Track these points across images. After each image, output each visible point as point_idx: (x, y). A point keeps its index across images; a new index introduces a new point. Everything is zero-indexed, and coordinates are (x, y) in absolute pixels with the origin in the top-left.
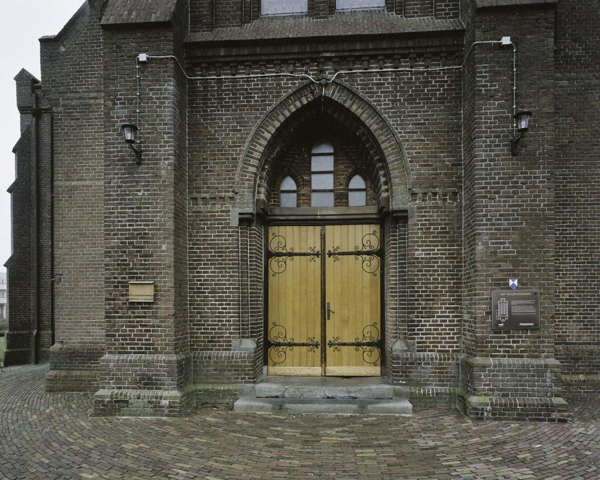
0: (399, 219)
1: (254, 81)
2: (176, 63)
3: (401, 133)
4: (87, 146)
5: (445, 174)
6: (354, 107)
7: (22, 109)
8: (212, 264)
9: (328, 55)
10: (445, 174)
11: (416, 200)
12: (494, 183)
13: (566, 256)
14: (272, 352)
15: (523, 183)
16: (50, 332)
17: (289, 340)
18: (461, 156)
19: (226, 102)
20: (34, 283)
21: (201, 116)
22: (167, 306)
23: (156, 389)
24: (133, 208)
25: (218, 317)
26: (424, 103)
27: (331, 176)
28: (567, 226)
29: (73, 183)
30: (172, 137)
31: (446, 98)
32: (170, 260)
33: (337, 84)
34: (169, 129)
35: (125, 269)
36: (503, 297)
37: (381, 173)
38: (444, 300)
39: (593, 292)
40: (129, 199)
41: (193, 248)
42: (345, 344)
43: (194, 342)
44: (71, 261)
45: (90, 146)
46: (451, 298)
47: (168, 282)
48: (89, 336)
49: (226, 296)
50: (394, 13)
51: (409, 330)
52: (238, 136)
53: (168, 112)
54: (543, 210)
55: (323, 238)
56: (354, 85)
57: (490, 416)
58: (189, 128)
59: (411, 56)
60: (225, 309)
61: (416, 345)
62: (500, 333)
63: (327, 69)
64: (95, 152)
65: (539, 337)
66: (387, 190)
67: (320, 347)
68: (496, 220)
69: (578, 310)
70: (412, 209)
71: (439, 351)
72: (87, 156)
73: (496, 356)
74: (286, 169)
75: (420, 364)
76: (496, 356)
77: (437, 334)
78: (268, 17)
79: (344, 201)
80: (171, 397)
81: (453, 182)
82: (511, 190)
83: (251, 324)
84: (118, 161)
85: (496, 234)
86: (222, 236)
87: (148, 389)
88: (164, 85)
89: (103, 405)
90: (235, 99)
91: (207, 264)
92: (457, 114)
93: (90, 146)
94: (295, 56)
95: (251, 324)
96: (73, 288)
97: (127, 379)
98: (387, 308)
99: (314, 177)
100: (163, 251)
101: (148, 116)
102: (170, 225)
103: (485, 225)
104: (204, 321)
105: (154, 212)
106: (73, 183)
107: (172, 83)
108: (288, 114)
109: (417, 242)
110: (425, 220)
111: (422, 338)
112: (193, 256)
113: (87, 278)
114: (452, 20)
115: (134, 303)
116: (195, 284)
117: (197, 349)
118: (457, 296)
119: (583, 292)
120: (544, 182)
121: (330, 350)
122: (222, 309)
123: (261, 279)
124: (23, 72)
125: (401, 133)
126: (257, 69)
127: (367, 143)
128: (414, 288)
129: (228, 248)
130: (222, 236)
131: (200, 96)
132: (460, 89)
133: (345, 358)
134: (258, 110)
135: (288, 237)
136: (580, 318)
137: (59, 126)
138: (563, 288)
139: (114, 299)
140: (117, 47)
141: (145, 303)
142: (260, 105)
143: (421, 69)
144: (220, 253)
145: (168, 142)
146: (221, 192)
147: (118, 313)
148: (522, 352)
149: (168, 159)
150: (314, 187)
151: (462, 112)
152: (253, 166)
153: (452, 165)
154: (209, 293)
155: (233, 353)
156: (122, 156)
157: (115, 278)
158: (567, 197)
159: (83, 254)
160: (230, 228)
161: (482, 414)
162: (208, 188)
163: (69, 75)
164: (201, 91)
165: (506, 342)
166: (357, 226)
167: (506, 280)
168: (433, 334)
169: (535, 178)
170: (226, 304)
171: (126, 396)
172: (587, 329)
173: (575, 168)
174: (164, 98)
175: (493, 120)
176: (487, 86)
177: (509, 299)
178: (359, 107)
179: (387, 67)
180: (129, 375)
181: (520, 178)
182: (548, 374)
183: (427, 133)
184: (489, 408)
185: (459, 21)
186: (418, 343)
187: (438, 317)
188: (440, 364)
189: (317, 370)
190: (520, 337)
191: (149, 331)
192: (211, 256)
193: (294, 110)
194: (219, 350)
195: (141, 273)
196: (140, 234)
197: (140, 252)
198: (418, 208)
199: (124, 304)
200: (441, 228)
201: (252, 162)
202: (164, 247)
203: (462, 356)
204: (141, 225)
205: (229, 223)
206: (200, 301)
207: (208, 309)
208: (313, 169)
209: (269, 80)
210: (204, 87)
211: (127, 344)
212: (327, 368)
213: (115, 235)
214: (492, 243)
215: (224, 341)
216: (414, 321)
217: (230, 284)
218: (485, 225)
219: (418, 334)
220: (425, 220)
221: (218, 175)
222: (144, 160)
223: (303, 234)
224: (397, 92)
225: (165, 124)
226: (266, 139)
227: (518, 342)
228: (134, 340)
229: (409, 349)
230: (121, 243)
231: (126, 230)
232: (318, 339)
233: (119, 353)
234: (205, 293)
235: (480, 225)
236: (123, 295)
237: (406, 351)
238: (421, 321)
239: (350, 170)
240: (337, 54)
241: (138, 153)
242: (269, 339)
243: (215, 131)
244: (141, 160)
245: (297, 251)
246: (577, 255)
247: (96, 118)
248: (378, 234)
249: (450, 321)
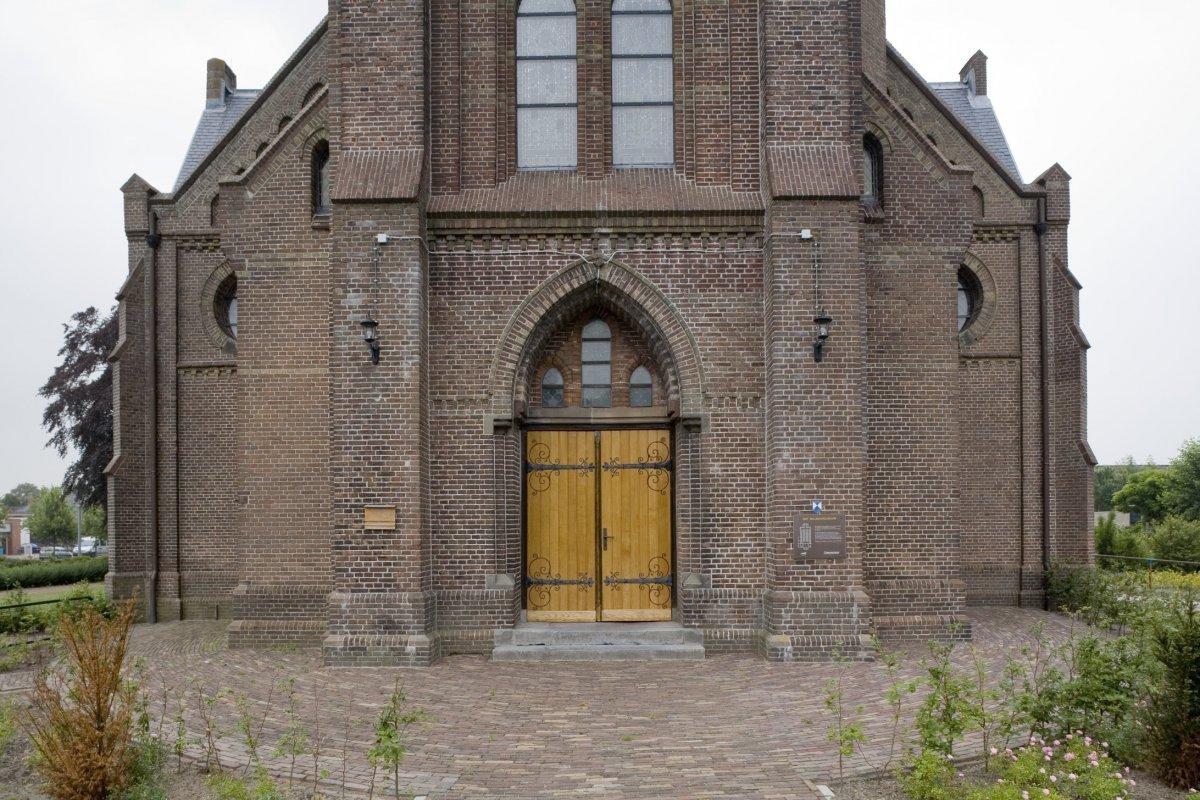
0: (693, 426)
1: (512, 258)
2: (421, 243)
3: (692, 325)
4: (282, 323)
5: (744, 375)
6: (636, 293)
7: (131, 235)
8: (460, 482)
9: (604, 230)
10: (746, 375)
11: (710, 405)
12: (795, 392)
13: (899, 469)
14: (532, 592)
15: (827, 393)
16: (175, 574)
17: (554, 576)
18: (763, 355)
19: (477, 283)
20: (149, 499)
21: (445, 298)
22: (410, 534)
23: (400, 633)
24: (368, 417)
25: (469, 547)
26: (719, 291)
27: (608, 367)
28: (900, 433)
29: (264, 372)
30: (416, 333)
31: (746, 286)
32: (414, 480)
33: (616, 265)
34: (414, 322)
35: (359, 490)
36: (805, 521)
37: (670, 370)
38: (744, 525)
39: (930, 514)
40: (364, 406)
41: (436, 462)
42: (626, 582)
43: (438, 578)
44: (259, 475)
45: (286, 322)
46: (753, 523)
47: (411, 505)
48: (285, 574)
49: (478, 522)
50: (684, 175)
51: (703, 562)
52: (493, 324)
53: (412, 303)
54: (850, 424)
55: (598, 446)
56: (635, 267)
57: (791, 655)
58: (430, 314)
59: (702, 235)
60: (477, 537)
61: (712, 579)
62: (803, 563)
63: (602, 247)
64: (293, 331)
65: (846, 567)
66: (677, 392)
67: (594, 585)
68: (798, 434)
69: (914, 537)
70: (706, 415)
71: (739, 586)
72: (282, 336)
73: (799, 589)
74: (549, 359)
75: (716, 602)
76: (799, 589)
77: (737, 566)
78: (528, 172)
79: (624, 399)
80: (418, 643)
81: (754, 385)
82: (815, 401)
83: (509, 556)
84: (351, 359)
85: (798, 450)
86: (473, 447)
87: (389, 633)
88: (407, 270)
89: (336, 653)
90: (489, 279)
91: (455, 482)
92: (758, 305)
93: (286, 322)
94: (564, 231)
95: (509, 556)
96: (264, 511)
97: (364, 622)
98: (679, 534)
99: (586, 369)
100: (407, 469)
101: (388, 306)
102: (415, 437)
103: (785, 440)
104: (451, 552)
105: (395, 422)
106: (264, 372)
107: (417, 268)
108: (554, 299)
109: (712, 456)
110: (722, 430)
111: (718, 571)
112: (436, 473)
113: (282, 497)
114: (751, 193)
115: (369, 531)
116: (439, 507)
117: (441, 588)
118: (760, 520)
119: (920, 514)
120: (850, 392)
121: (607, 590)
122: (474, 537)
123: (518, 498)
124: (135, 179)
125: (692, 325)
126: (516, 243)
127: (653, 333)
128: (708, 511)
129: (481, 462)
130: (473, 447)
131: (445, 274)
132: (761, 275)
133: (626, 599)
134: (518, 293)
135: (553, 446)
136: (916, 546)
137: (245, 296)
138: (896, 510)
139: (346, 527)
140: (351, 224)
141: (385, 531)
142: (520, 288)
143: (716, 251)
144: (470, 468)
145: (411, 338)
146: (472, 393)
147: (350, 543)
148: (827, 584)
149: (411, 358)
150: (586, 381)
151: (764, 302)
152: (511, 361)
153: (753, 365)
154: (457, 517)
155: (487, 593)
156: (355, 354)
157: (347, 501)
158: (900, 397)
159: (277, 466)
160: (482, 437)
161: (782, 655)
162: (455, 387)
163: (259, 229)
164: (446, 269)
165: (809, 573)
166: (641, 431)
167: (808, 502)
168: (731, 566)
169: (841, 387)
170: (478, 532)
171: (363, 642)
172: (924, 559)
173: (909, 361)
174: (407, 286)
175: (793, 321)
176: (786, 282)
177: (813, 524)
178: (641, 293)
179: (675, 247)
180: (365, 617)
181: (824, 387)
182: (855, 608)
183: (723, 325)
184: (789, 648)
185: (759, 195)
186: (714, 576)
187: (738, 545)
188: (740, 602)
189: (591, 615)
190: (825, 567)
191: (390, 564)
192: (459, 472)
193: (562, 294)
194: (470, 588)
195: (379, 495)
196: (378, 448)
197: (378, 469)
198: (713, 415)
199: (358, 532)
200: (741, 440)
201: (510, 356)
202: (407, 464)
203: (765, 591)
204: (378, 437)
205: (481, 432)
206: (446, 527)
207: (456, 537)
208: (585, 358)
209: (530, 258)
210: (450, 264)
211: (362, 580)
212: (605, 611)
213: (346, 448)
214: (794, 461)
215: (476, 577)
216: (709, 551)
217: (483, 507)
218: (785, 440)
219: (714, 566)
220: (722, 430)
221: (468, 372)
222: (382, 359)
223: (572, 441)
224: (687, 276)
225: (408, 317)
226: (527, 329)
227: (823, 573)
228: (371, 575)
229: (704, 582)
230: (355, 458)
231: (361, 443)
232: (591, 575)
233: (353, 591)
234: (451, 517)
235: (779, 440)
236: (356, 522)
237: (699, 587)
238: (717, 551)
239: (632, 361)
240: (616, 230)
241: (376, 352)
242: (528, 575)
243: (464, 318)
244: (379, 359)
245: (564, 462)
246: (912, 469)
247: (294, 286)
248: (668, 442)
249: (751, 550)
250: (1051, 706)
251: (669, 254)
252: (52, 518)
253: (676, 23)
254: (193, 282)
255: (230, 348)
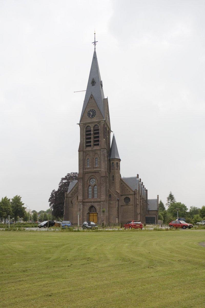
250: (46, 213)
251: (96, 204)
252: (45, 217)
253: (92, 195)
254: (70, 200)
255: (72, 205)
